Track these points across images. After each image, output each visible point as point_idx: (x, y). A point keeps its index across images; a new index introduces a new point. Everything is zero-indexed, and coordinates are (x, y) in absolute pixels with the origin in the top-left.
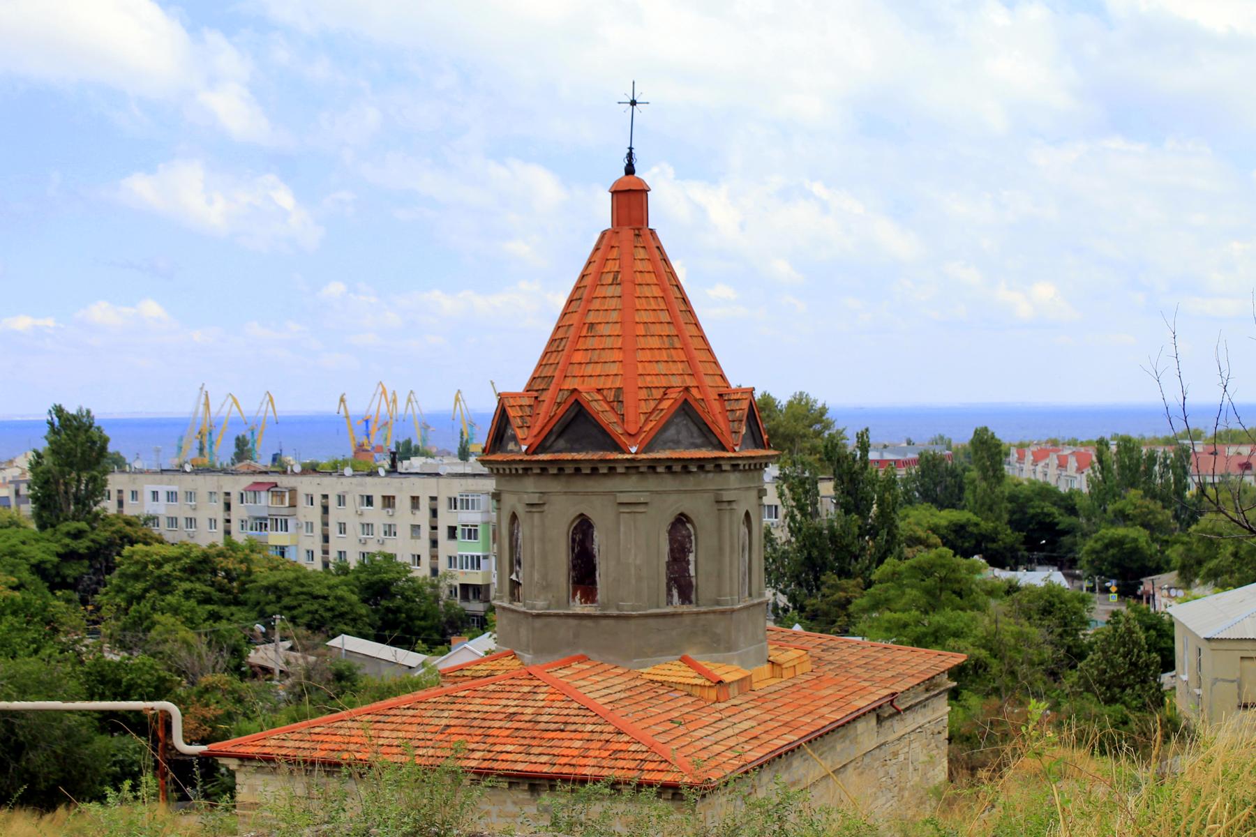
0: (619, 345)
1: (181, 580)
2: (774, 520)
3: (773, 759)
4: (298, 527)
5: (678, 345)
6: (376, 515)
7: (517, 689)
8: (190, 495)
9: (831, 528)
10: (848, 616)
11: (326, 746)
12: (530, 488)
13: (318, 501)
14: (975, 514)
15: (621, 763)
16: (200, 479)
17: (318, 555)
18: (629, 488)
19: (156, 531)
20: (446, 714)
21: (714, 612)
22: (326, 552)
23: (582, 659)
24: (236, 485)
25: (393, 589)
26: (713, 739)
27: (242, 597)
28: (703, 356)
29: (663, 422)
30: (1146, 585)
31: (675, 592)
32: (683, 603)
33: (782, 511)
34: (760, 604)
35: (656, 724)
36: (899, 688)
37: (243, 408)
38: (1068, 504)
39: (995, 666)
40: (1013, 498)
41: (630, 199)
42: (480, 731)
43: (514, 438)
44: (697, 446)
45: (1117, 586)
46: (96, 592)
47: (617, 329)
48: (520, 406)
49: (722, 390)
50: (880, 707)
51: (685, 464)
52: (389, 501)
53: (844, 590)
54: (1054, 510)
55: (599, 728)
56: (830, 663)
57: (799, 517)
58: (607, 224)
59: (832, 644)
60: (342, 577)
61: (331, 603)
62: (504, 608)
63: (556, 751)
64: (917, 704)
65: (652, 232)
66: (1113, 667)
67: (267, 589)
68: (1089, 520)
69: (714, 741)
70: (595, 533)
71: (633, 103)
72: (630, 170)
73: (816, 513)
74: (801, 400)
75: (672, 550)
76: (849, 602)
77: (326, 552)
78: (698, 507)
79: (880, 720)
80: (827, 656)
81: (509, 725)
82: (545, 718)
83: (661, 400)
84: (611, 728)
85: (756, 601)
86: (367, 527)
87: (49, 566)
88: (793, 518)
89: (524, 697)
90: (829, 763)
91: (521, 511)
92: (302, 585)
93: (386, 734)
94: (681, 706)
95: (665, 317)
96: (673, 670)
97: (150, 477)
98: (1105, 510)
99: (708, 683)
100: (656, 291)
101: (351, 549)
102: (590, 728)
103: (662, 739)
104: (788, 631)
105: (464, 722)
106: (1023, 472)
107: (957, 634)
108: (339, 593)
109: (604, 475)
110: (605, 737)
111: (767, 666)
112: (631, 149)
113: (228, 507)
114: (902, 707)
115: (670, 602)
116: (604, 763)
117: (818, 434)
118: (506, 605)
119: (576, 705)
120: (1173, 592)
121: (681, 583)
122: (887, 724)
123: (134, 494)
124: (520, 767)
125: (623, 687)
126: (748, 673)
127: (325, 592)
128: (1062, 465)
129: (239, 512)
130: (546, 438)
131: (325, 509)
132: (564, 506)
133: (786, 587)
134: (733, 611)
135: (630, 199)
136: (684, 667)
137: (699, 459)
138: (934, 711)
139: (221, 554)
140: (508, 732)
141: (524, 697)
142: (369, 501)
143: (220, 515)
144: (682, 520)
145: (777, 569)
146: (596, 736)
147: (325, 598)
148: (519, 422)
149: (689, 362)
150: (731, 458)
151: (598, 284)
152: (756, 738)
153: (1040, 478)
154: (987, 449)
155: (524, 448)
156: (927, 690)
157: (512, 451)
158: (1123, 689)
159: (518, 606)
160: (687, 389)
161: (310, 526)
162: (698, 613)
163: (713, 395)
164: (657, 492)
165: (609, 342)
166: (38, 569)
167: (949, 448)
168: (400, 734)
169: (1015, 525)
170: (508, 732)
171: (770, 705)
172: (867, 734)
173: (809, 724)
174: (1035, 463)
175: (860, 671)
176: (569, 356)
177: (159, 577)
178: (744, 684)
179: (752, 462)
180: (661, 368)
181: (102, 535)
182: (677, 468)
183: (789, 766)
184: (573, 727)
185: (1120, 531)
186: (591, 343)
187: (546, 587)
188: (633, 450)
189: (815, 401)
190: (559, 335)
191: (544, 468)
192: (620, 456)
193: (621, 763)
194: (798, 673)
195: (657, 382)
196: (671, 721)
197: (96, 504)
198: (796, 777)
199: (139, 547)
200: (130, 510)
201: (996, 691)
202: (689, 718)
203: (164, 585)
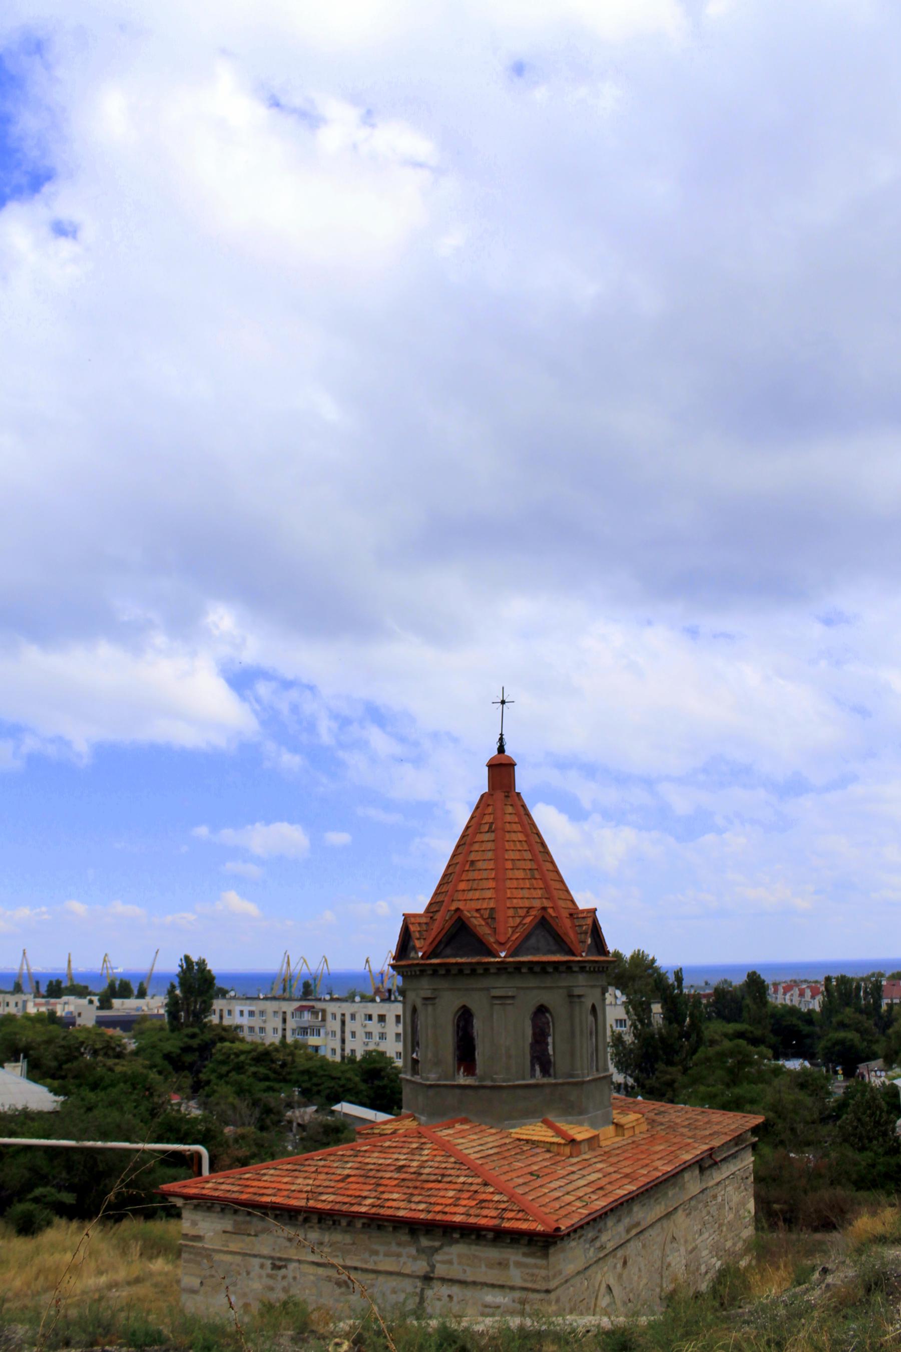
0: (493, 876)
1: (251, 1065)
2: (624, 1029)
3: (616, 1207)
4: (327, 1034)
5: (538, 876)
6: (374, 1026)
7: (407, 1145)
8: (262, 1013)
9: (660, 1033)
10: (674, 1091)
11: (251, 1190)
12: (425, 987)
13: (339, 1017)
14: (750, 1025)
15: (485, 1212)
16: (268, 1003)
17: (338, 1051)
18: (501, 986)
19: (241, 1035)
20: (349, 1165)
21: (568, 1083)
22: (343, 1050)
23: (464, 1121)
24: (289, 1007)
25: (383, 1074)
26: (564, 1190)
27: (288, 1077)
28: (552, 875)
29: (526, 933)
30: (862, 1068)
31: (537, 1068)
32: (544, 1076)
33: (629, 1023)
34: (605, 1077)
35: (518, 1177)
36: (716, 1143)
37: (310, 967)
38: (808, 1018)
39: (780, 1126)
40: (773, 1016)
41: (501, 770)
42: (374, 1181)
43: (414, 948)
44: (553, 953)
45: (843, 1069)
46: (200, 1072)
47: (491, 865)
48: (419, 924)
49: (572, 911)
50: (702, 1159)
51: (543, 965)
52: (382, 1018)
53: (670, 1074)
54: (799, 1023)
55: (470, 1180)
56: (662, 1124)
57: (639, 1027)
58: (486, 789)
59: (662, 1109)
60: (350, 1066)
61: (343, 1082)
62: (407, 1080)
63: (433, 1200)
64: (729, 1156)
65: (518, 794)
66: (862, 1125)
67: (303, 1073)
68: (821, 1027)
69: (566, 1193)
70: (475, 1021)
71: (503, 702)
72: (501, 750)
73: (650, 1024)
74: (639, 954)
75: (534, 1034)
76: (673, 1081)
77: (343, 1050)
78: (554, 999)
79: (702, 1170)
80: (659, 1119)
81: (396, 1175)
82: (427, 1170)
83: (524, 917)
84: (479, 1180)
85: (602, 1075)
86: (369, 1034)
87: (174, 1055)
88: (636, 1028)
89: (412, 1152)
90: (663, 1207)
91: (419, 1003)
92: (325, 1070)
93: (299, 1181)
94: (541, 1160)
95: (528, 855)
96: (537, 1131)
97: (239, 1002)
98: (831, 1022)
99: (563, 1141)
100: (521, 837)
101: (358, 1047)
102: (462, 1179)
103: (520, 1191)
104: (631, 1100)
105: (362, 1172)
106: (779, 999)
107: (752, 1102)
108: (348, 1075)
109: (481, 974)
110: (474, 1188)
111: (611, 1128)
112: (502, 735)
113: (284, 1021)
114: (719, 1159)
115: (533, 1075)
116: (472, 1211)
117: (651, 975)
118: (409, 1077)
119: (452, 1160)
120: (878, 1073)
121: (541, 1059)
122: (708, 1173)
123: (230, 1012)
124: (401, 1213)
125: (495, 1144)
126: (596, 1132)
127: (339, 1075)
128: (802, 994)
129: (291, 1023)
130: (437, 946)
131: (343, 1023)
132: (450, 1002)
133: (633, 1072)
134: (583, 1083)
135: (501, 770)
136: (544, 1128)
137: (554, 962)
138: (742, 1161)
139: (277, 1050)
140: (396, 1182)
141: (412, 1152)
142: (370, 1017)
143: (280, 1026)
144: (541, 1010)
145: (626, 1060)
146: (466, 1187)
147: (339, 1079)
148: (417, 935)
149: (547, 888)
150: (579, 962)
151: (478, 831)
152: (601, 1188)
153: (788, 1002)
154: (755, 984)
155: (420, 954)
156: (736, 1145)
157: (413, 959)
158: (870, 1141)
159: (417, 1078)
160: (544, 909)
161: (334, 1033)
162: (556, 1085)
163: (565, 914)
164: (522, 988)
165: (485, 875)
166: (167, 1057)
167: (731, 986)
168: (311, 1182)
169: (775, 1032)
170: (396, 1182)
171: (614, 1160)
172: (692, 1184)
173: (645, 1176)
174: (785, 993)
175: (685, 1130)
176: (456, 885)
177: (238, 1063)
178: (593, 1142)
179: (595, 965)
180: (525, 893)
181: (208, 1036)
182: (537, 969)
183: (630, 1211)
184: (449, 1179)
185: (841, 1035)
186: (472, 875)
187: (437, 1063)
188: (503, 955)
189: (648, 955)
190: (449, 872)
191: (435, 971)
192: (492, 960)
193: (485, 1212)
194: (637, 1132)
195: (521, 903)
196: (531, 1174)
197: (206, 1017)
198: (636, 1220)
199: (227, 1044)
200: (227, 1022)
201: (782, 1142)
202: (547, 1170)
203: (239, 1068)
